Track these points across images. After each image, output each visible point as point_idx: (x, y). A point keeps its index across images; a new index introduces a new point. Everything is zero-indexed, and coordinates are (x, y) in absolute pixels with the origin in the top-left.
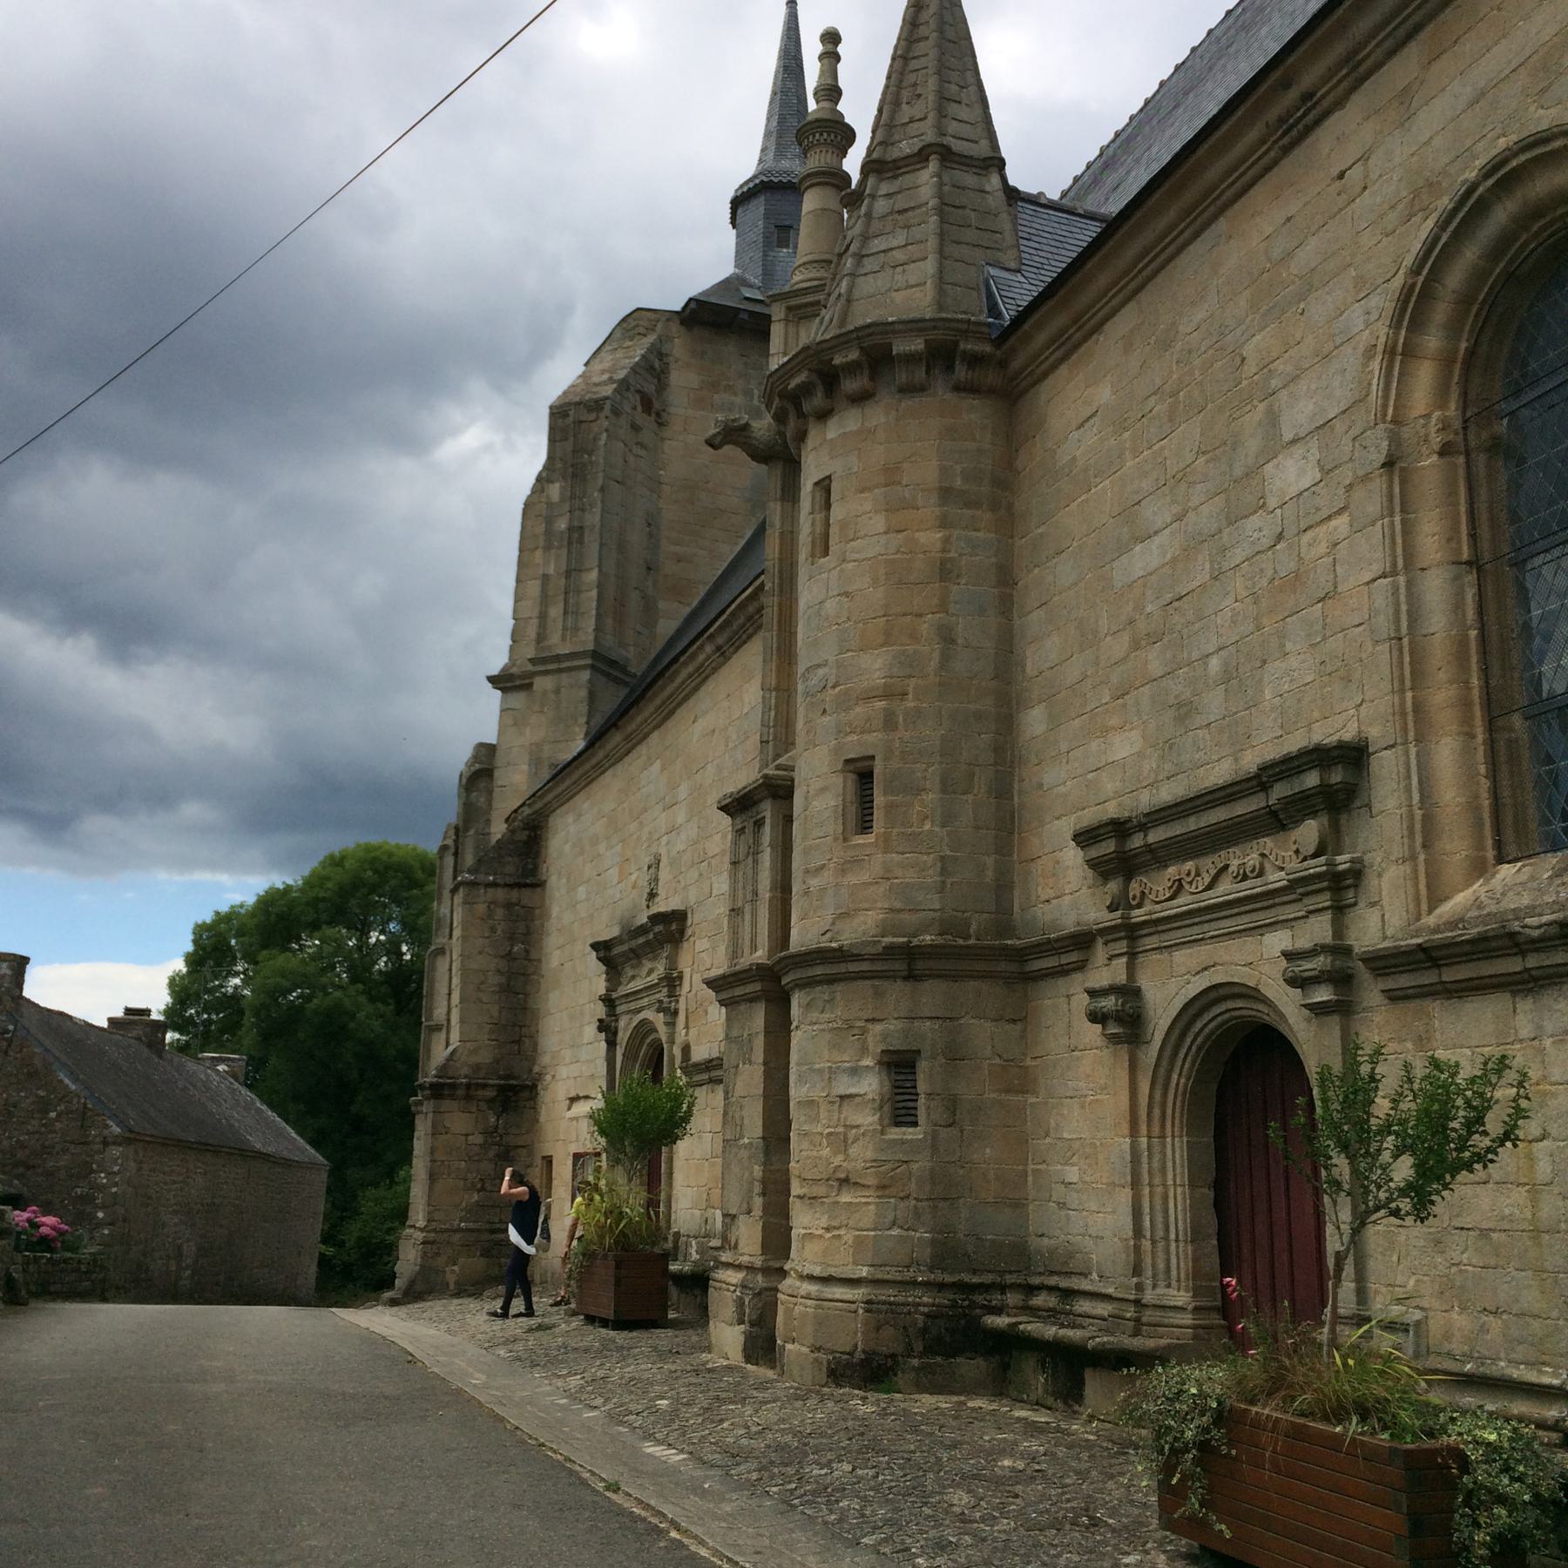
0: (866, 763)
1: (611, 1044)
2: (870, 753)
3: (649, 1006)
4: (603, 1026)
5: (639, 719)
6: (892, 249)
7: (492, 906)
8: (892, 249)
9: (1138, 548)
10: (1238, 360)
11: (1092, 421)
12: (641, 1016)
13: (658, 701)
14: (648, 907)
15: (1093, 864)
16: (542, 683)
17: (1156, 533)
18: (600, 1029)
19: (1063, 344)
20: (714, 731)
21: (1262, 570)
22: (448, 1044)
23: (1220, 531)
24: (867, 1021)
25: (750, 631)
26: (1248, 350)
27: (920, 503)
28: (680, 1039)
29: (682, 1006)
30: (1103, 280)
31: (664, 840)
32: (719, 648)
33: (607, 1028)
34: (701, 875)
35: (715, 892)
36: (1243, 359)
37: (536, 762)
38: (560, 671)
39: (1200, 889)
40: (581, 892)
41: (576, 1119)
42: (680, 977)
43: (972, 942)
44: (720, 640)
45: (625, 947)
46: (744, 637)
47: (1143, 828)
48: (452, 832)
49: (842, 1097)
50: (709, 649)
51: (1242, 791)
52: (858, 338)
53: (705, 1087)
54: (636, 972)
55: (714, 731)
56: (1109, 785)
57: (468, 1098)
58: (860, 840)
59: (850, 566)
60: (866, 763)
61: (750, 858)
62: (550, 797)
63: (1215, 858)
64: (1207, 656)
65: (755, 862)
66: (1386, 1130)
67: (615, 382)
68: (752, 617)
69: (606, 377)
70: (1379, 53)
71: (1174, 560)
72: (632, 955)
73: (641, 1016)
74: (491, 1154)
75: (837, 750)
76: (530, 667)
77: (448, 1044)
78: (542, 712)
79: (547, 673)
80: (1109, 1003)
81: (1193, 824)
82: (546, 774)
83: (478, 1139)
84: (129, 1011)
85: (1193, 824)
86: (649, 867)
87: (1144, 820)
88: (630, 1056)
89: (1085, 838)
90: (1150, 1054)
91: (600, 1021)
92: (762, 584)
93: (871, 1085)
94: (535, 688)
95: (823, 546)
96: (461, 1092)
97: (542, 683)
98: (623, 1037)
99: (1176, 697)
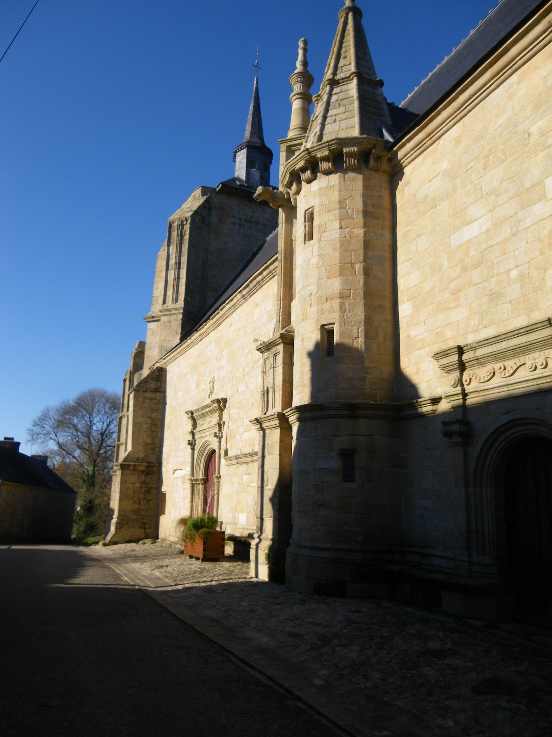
0: (330, 326)
1: (193, 449)
2: (333, 322)
3: (209, 435)
4: (190, 443)
5: (206, 327)
6: (339, 114)
7: (145, 399)
8: (339, 114)
9: (466, 228)
10: (526, 135)
11: (436, 179)
12: (205, 439)
13: (215, 319)
14: (209, 397)
15: (443, 368)
16: (164, 319)
17: (476, 220)
18: (189, 444)
19: (249, 294)
20: (240, 329)
21: (544, 227)
22: (126, 450)
23: (516, 213)
24: (332, 436)
25: (258, 288)
26: (534, 130)
27: (355, 216)
28: (223, 446)
29: (224, 435)
30: (444, 114)
31: (217, 372)
32: (243, 296)
33: (192, 444)
34: (233, 384)
35: (239, 390)
36: (529, 135)
37: (161, 348)
38: (170, 315)
39: (507, 375)
40: (180, 394)
41: (177, 478)
42: (224, 423)
43: (378, 402)
44: (244, 292)
45: (200, 413)
46: (255, 291)
47: (474, 348)
48: (129, 373)
49: (320, 469)
50: (239, 296)
51: (533, 329)
52: (329, 145)
53: (234, 466)
54: (204, 422)
55: (240, 329)
56: (449, 333)
57: (134, 470)
58: (328, 359)
59: (323, 243)
60: (330, 326)
61: (272, 370)
62: (168, 359)
63: (516, 360)
64: (509, 271)
65: (274, 372)
66: (149, 470)
67: (192, 211)
68: (259, 282)
69: (189, 209)
70: (268, 279)
71: (487, 231)
72: (202, 416)
73: (205, 439)
74: (143, 490)
75: (317, 321)
76: (160, 314)
77: (126, 450)
78: (164, 329)
79: (166, 315)
80: (455, 428)
81: (504, 345)
82: (164, 353)
83: (138, 485)
84: (6, 438)
85: (504, 345)
86: (210, 382)
87: (474, 346)
88: (201, 454)
89: (439, 355)
90: (475, 451)
91: (189, 441)
92: (277, 258)
93: (335, 464)
94: (161, 320)
95: (309, 236)
96: (132, 468)
97: (164, 319)
98: (197, 448)
99: (490, 291)
